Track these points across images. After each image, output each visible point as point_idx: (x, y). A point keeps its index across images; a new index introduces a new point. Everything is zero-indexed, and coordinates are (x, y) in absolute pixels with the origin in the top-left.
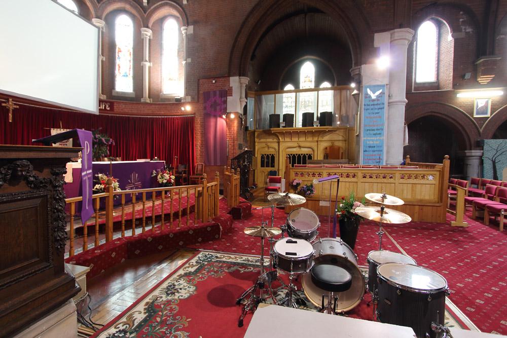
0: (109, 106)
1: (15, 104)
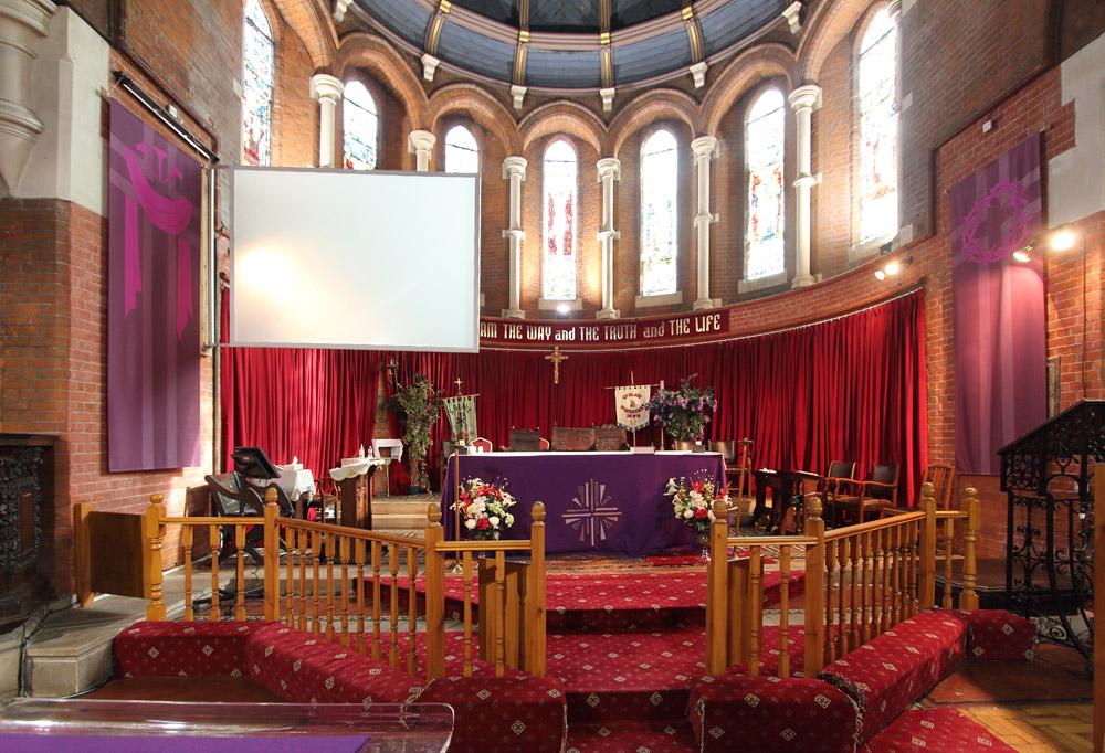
0: (720, 322)
1: (564, 354)
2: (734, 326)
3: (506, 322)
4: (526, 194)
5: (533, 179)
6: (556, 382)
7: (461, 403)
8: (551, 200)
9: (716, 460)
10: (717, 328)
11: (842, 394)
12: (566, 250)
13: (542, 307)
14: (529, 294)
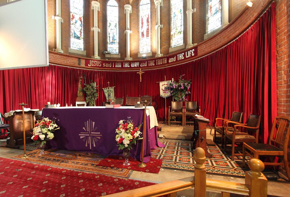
1: (143, 71)
2: (200, 53)
3: (124, 62)
4: (132, 18)
5: (135, 12)
6: (141, 81)
7: (109, 90)
8: (142, 19)
9: (142, 112)
10: (193, 55)
11: (238, 78)
12: (147, 35)
13: (139, 56)
14: (134, 52)
